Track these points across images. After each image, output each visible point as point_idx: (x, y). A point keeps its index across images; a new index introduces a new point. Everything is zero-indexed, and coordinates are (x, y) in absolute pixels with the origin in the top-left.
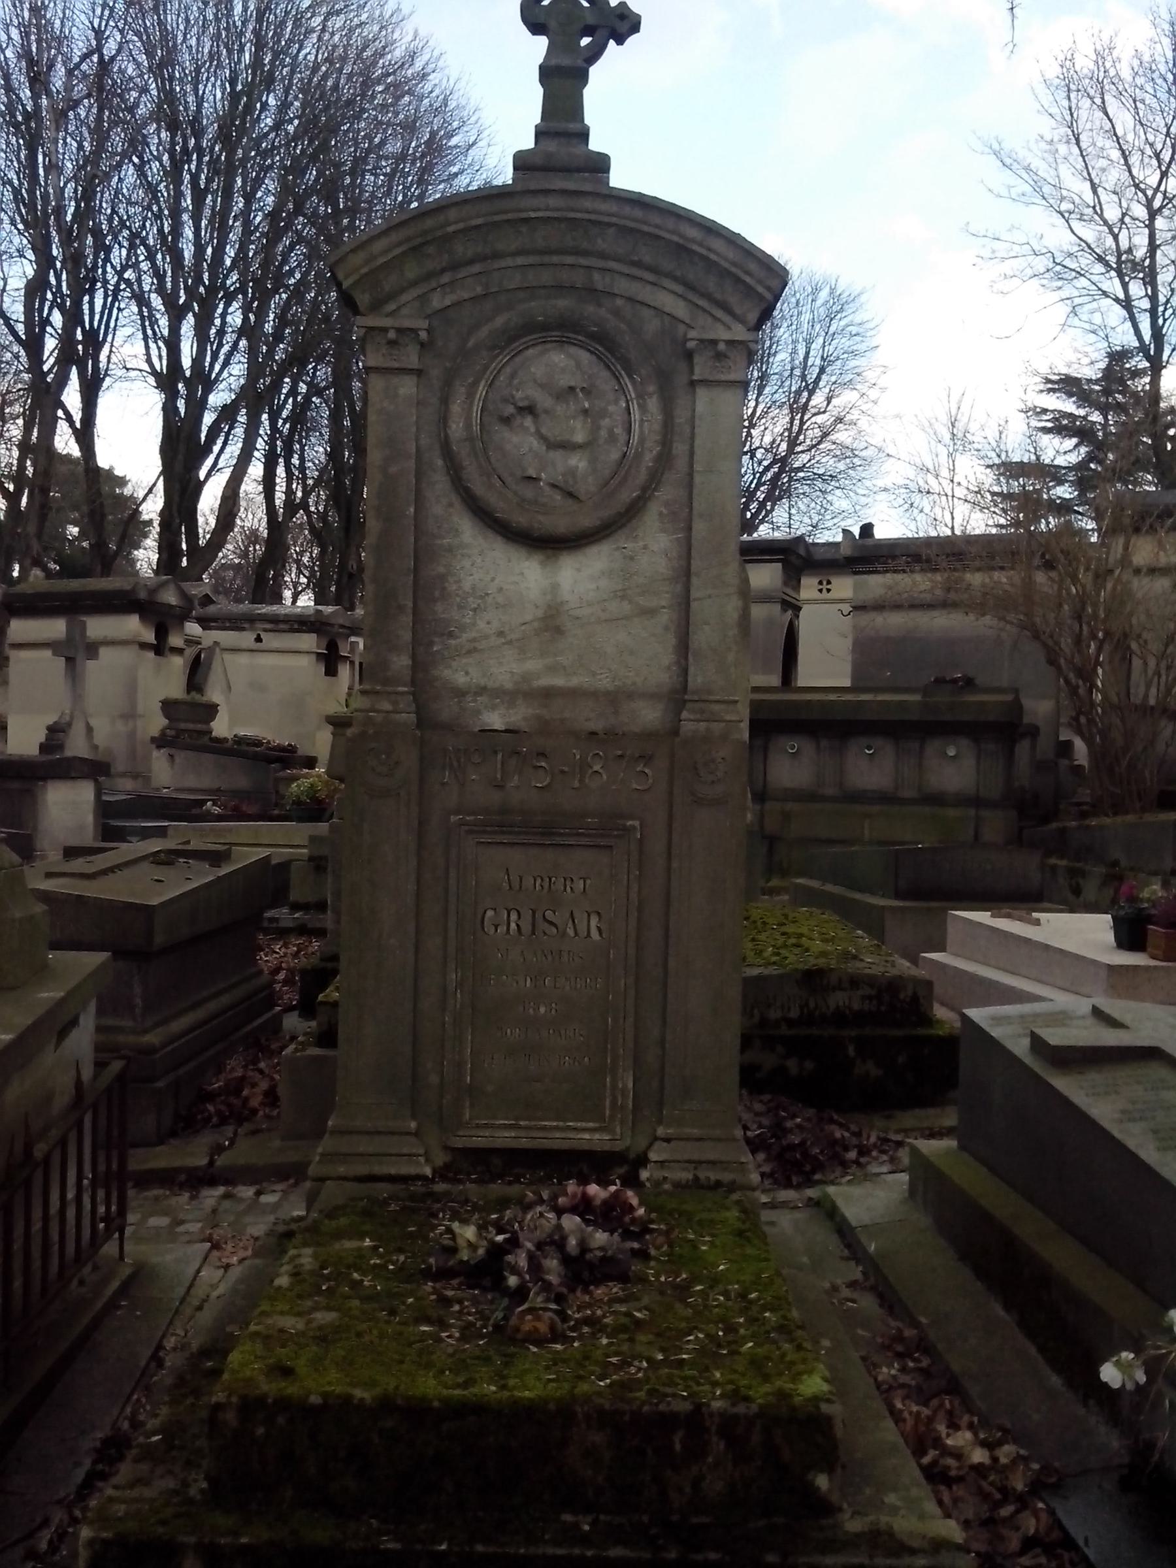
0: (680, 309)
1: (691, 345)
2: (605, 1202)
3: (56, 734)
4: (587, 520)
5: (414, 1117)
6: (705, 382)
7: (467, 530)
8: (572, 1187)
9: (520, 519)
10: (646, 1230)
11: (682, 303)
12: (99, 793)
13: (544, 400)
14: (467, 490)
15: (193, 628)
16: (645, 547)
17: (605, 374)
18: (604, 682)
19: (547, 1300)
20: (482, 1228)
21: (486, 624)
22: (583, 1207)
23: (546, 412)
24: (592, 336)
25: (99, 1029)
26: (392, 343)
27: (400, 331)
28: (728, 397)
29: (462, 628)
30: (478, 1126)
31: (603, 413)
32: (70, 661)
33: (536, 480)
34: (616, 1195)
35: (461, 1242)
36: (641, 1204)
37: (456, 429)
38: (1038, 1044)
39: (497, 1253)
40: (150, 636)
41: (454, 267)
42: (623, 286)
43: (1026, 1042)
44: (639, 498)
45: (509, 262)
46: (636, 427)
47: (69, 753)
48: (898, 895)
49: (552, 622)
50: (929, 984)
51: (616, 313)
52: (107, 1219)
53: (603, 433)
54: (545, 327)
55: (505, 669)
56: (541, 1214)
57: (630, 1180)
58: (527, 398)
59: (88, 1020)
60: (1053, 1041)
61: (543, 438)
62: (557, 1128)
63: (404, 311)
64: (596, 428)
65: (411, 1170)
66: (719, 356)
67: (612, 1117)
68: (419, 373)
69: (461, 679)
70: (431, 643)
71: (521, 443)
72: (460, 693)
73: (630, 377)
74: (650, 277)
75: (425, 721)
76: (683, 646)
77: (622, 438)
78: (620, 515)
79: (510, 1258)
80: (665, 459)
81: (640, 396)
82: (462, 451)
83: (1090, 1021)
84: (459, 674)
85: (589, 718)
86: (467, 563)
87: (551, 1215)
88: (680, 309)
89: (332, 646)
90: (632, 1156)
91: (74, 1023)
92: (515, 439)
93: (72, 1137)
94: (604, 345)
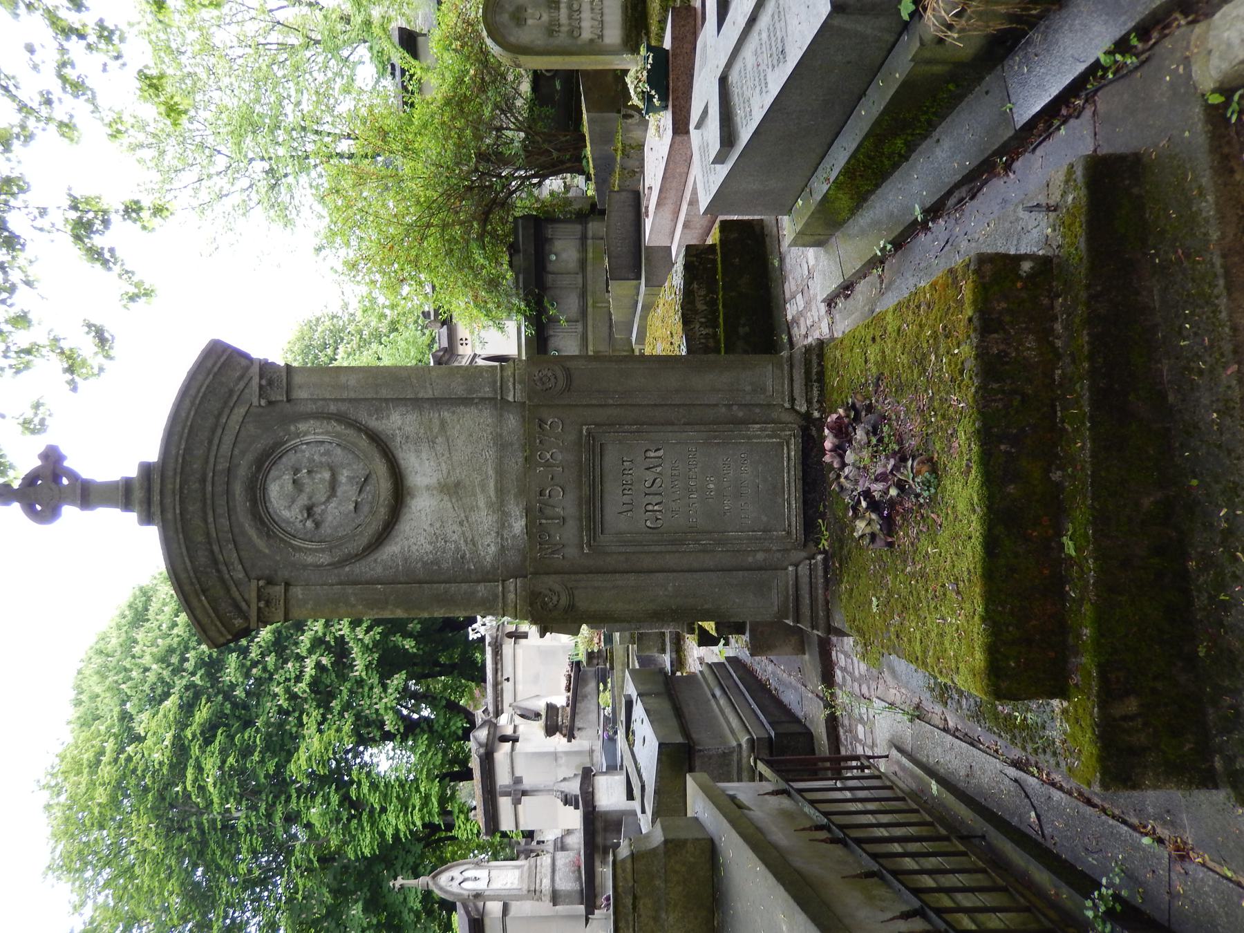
0: (241, 411)
1: (263, 402)
2: (836, 436)
3: (567, 800)
4: (381, 468)
5: (786, 569)
6: (288, 392)
7: (392, 550)
8: (827, 459)
9: (383, 512)
10: (854, 406)
11: (236, 411)
12: (603, 773)
13: (303, 500)
14: (364, 550)
15: (503, 720)
16: (400, 429)
17: (284, 460)
18: (490, 454)
19: (905, 467)
20: (856, 515)
21: (454, 532)
22: (839, 450)
23: (310, 498)
24: (259, 469)
25: (740, 780)
26: (268, 603)
27: (259, 599)
28: (298, 379)
29: (458, 549)
30: (790, 525)
31: (311, 460)
32: (524, 793)
33: (356, 503)
34: (830, 429)
35: (868, 530)
36: (836, 412)
37: (324, 559)
38: (720, 159)
39: (874, 506)
40: (508, 745)
41: (215, 562)
42: (226, 448)
43: (718, 166)
44: (366, 434)
45: (212, 526)
46: (320, 438)
47: (578, 792)
48: (639, 278)
49: (451, 489)
50: (688, 247)
51: (243, 453)
52: (862, 768)
53: (323, 459)
54: (254, 502)
55: (485, 519)
56: (846, 477)
57: (821, 423)
58: (301, 512)
59: (732, 787)
60: (718, 146)
61: (328, 499)
62: (789, 472)
63: (246, 596)
64: (321, 465)
65: (820, 568)
66: (270, 383)
67: (779, 437)
68: (287, 585)
69: (493, 549)
70: (469, 570)
71: (335, 513)
72: (503, 549)
73: (286, 442)
74: (219, 431)
75: (517, 573)
76: (466, 401)
77: (327, 446)
78: (378, 445)
79: (877, 495)
80: (341, 418)
81: (298, 435)
82: (338, 554)
83: (703, 129)
84: (489, 549)
85: (515, 463)
86: (414, 548)
87: (847, 470)
88: (241, 411)
89: (510, 635)
90: (803, 423)
91: (733, 798)
92: (330, 518)
93: (810, 796)
94: (265, 461)
